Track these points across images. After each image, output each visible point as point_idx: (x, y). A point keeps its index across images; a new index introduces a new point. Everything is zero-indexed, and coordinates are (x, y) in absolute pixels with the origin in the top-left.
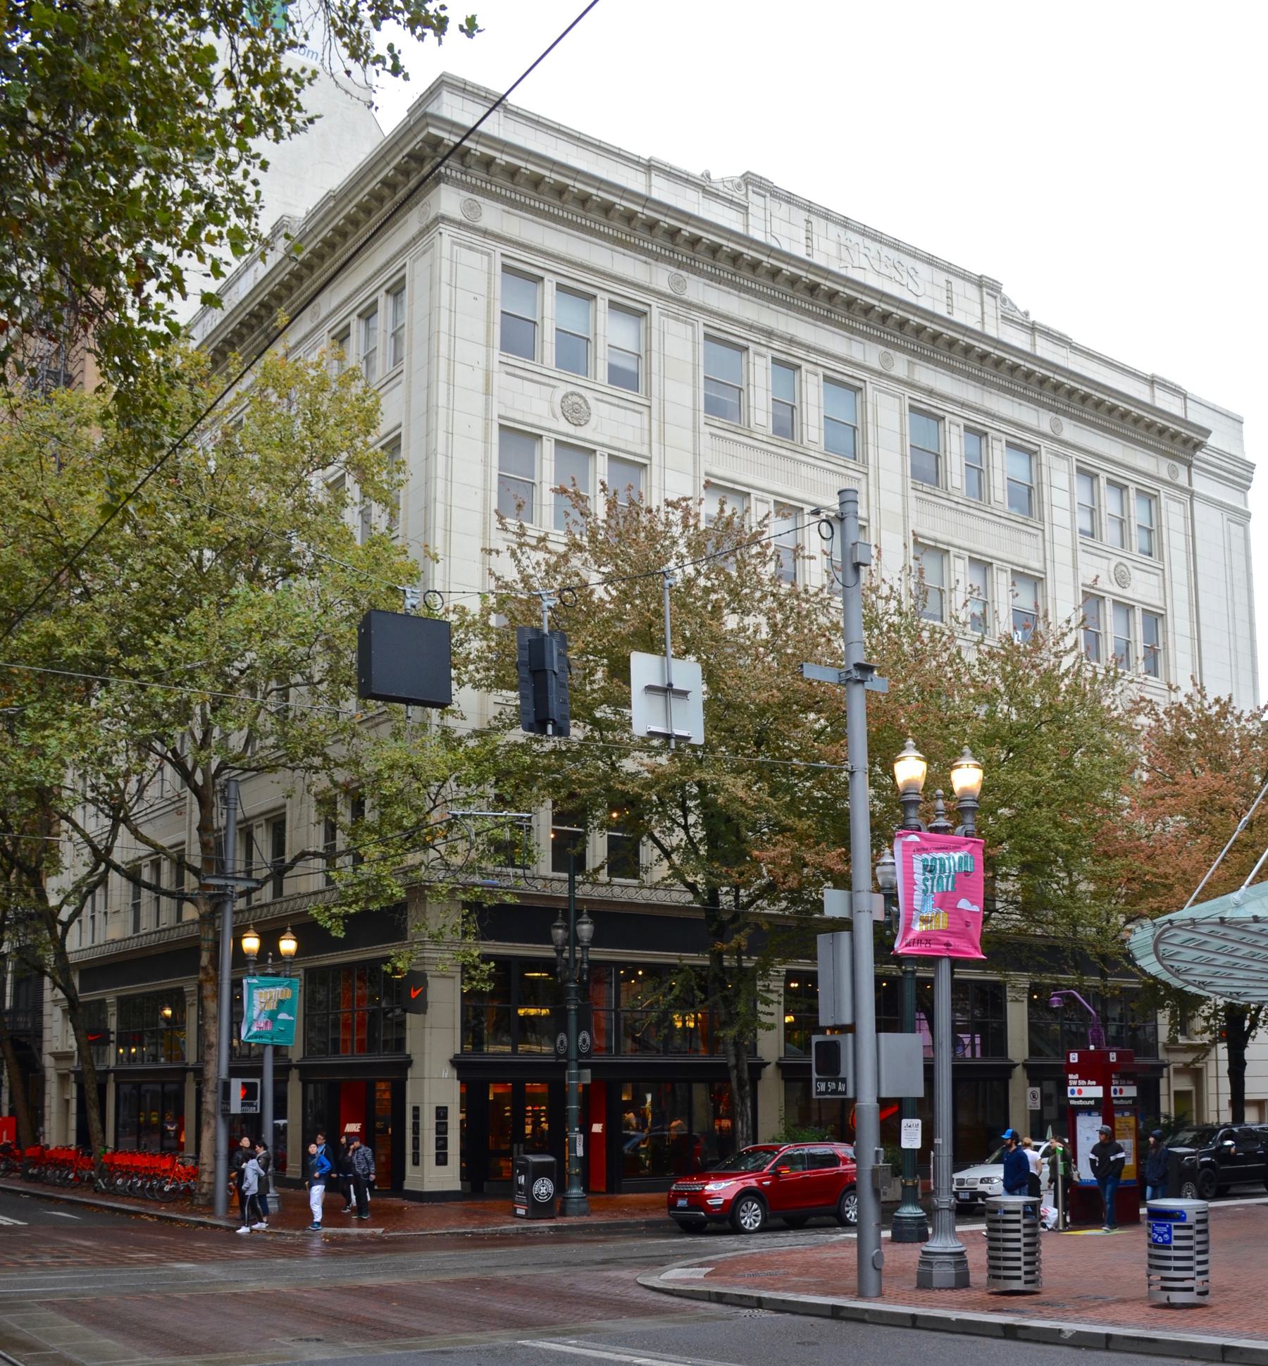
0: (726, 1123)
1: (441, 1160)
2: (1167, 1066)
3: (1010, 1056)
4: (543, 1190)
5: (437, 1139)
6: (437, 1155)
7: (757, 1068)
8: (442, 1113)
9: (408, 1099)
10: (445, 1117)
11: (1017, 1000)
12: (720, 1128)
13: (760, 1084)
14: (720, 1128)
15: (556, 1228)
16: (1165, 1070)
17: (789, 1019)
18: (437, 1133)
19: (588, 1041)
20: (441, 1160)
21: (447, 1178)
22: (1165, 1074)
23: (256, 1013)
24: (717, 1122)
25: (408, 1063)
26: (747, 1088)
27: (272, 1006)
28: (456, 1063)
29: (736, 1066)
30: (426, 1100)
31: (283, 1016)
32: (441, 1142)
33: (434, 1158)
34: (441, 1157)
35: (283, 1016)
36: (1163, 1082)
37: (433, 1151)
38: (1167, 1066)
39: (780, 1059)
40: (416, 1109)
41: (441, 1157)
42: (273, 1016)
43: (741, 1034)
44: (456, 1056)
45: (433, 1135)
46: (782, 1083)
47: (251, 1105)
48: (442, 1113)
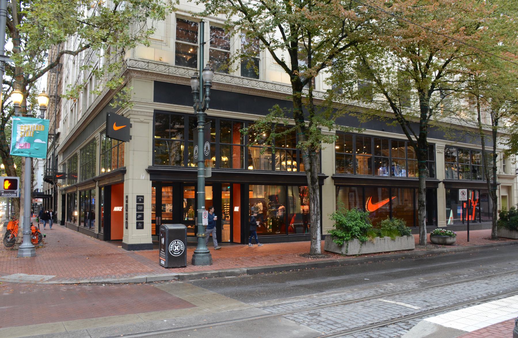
0: (306, 207)
1: (140, 225)
2: (499, 184)
3: (437, 178)
4: (177, 248)
5: (137, 214)
6: (137, 223)
7: (322, 178)
8: (140, 200)
9: (124, 193)
10: (143, 201)
11: (440, 153)
12: (303, 210)
13: (323, 187)
14: (303, 210)
15: (179, 278)
16: (498, 186)
17: (337, 147)
18: (137, 210)
19: (209, 148)
20: (140, 225)
21: (145, 236)
22: (498, 188)
23: (18, 138)
24: (302, 207)
25: (123, 172)
26: (317, 183)
27: (30, 134)
28: (150, 171)
29: (310, 170)
30: (130, 191)
31: (37, 141)
32: (140, 216)
33: (135, 226)
34: (140, 225)
35: (37, 141)
36: (497, 192)
37: (135, 221)
38: (499, 184)
39: (333, 175)
40: (127, 197)
41: (140, 225)
42: (30, 141)
43: (312, 145)
44: (149, 167)
45: (135, 212)
46: (334, 187)
47: (13, 193)
48: (140, 200)
